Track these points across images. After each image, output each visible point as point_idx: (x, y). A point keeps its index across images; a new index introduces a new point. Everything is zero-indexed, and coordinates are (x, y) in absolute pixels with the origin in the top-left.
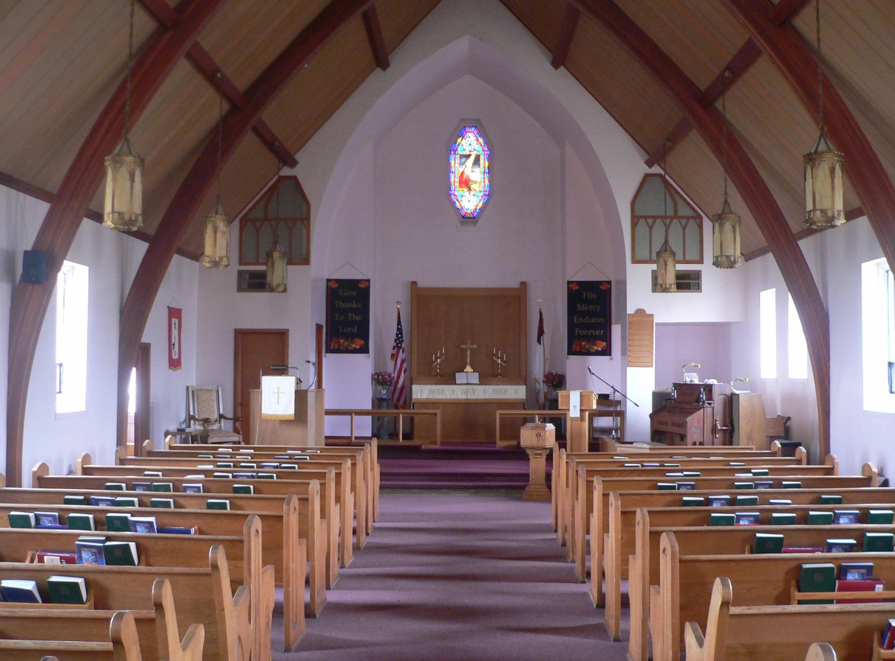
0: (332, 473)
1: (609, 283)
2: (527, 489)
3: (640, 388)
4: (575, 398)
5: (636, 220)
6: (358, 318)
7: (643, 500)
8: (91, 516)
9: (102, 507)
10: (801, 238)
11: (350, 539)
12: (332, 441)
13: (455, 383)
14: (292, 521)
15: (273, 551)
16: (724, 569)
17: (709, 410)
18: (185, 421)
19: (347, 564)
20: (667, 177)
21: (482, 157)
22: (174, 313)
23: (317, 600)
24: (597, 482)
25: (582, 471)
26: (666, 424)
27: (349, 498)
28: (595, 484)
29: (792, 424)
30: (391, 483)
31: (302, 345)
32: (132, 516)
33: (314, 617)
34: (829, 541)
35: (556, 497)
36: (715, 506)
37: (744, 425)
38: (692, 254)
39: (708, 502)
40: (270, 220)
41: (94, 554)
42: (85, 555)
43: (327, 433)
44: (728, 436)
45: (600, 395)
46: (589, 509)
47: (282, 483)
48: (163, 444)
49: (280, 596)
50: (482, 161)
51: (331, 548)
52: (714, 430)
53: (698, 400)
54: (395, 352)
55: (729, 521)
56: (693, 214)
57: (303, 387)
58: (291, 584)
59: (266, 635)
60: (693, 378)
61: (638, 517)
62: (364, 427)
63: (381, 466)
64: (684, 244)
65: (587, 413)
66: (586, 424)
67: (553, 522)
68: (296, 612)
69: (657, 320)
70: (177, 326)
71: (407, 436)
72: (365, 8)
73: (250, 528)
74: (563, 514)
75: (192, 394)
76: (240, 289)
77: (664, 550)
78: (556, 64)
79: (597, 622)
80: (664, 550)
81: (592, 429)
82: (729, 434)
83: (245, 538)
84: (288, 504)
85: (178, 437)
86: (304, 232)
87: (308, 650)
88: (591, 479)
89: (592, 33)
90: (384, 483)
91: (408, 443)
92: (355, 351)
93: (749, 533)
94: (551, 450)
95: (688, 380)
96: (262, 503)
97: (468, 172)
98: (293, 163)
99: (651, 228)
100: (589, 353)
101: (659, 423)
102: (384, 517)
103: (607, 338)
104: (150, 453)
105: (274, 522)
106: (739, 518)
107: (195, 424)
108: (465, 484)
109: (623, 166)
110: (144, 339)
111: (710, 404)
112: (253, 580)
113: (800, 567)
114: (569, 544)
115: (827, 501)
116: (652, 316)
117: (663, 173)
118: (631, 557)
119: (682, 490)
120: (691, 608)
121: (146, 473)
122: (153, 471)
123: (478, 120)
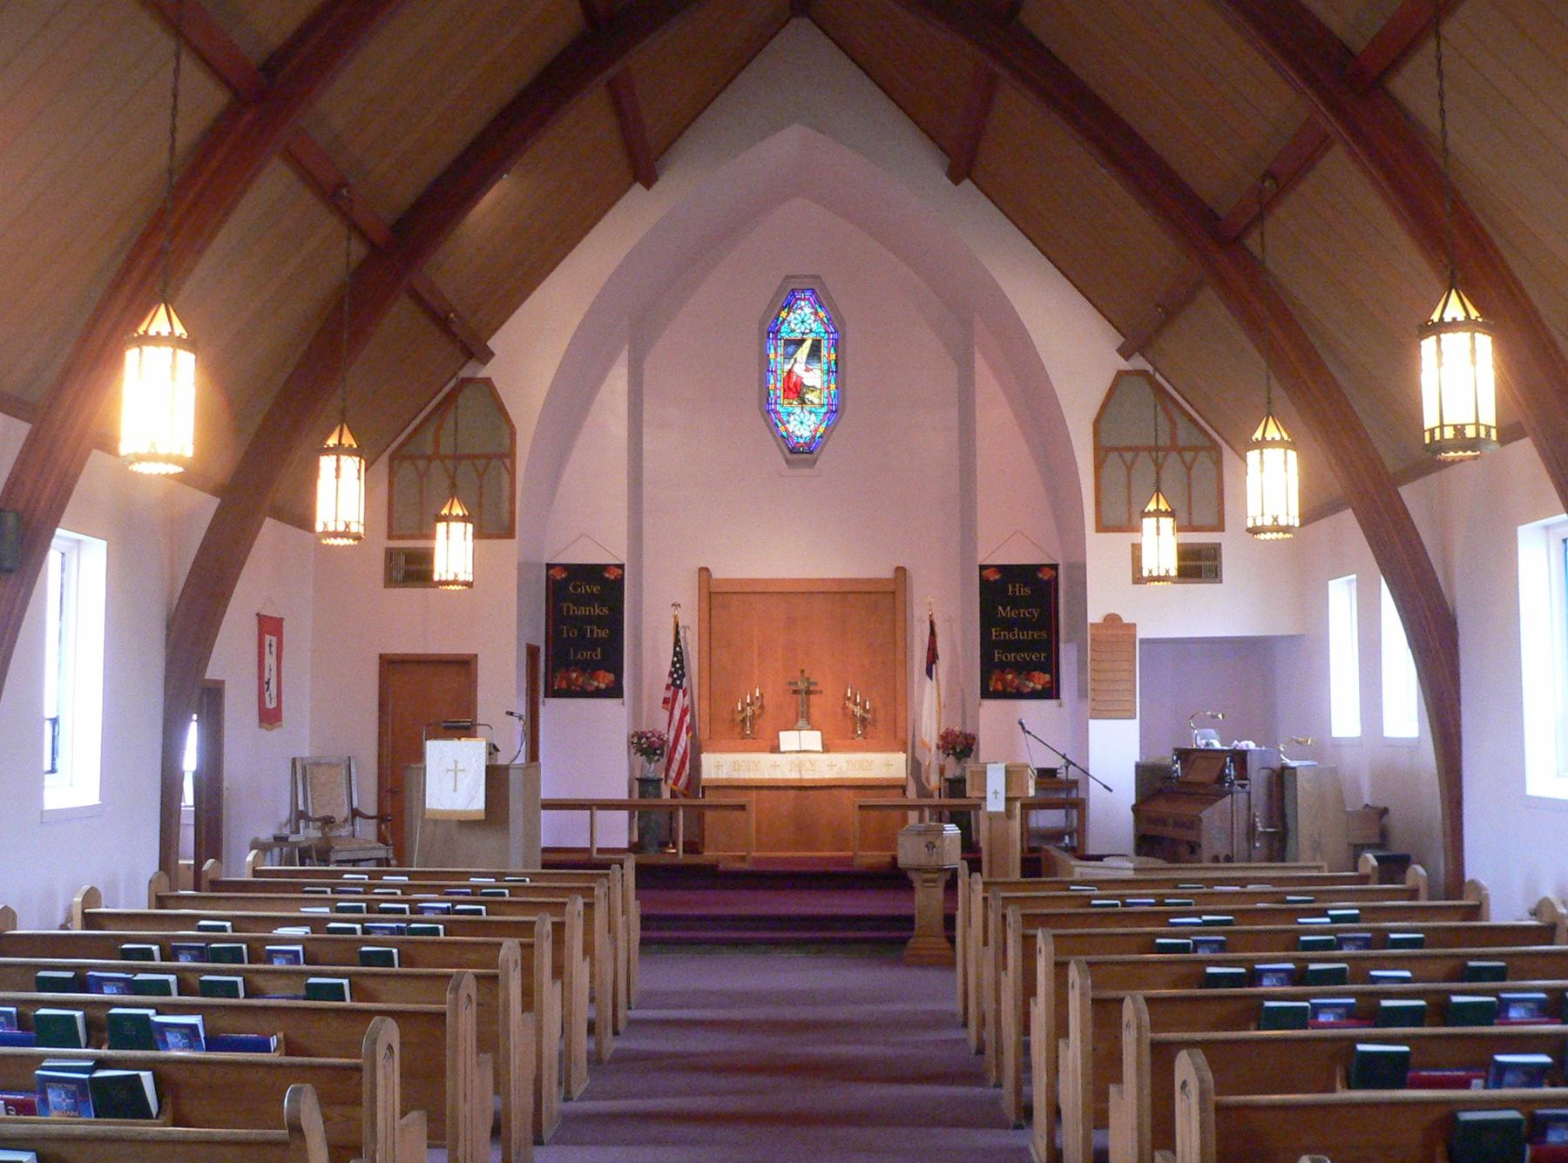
0: (544, 924)
1: (1055, 567)
2: (911, 943)
3: (1114, 754)
4: (996, 781)
6: (603, 634)
7: (1135, 975)
8: (78, 1014)
9: (108, 995)
10: (1401, 483)
11: (582, 1044)
12: (559, 861)
13: (775, 749)
14: (464, 1023)
17: (1241, 797)
18: (290, 820)
19: (577, 1091)
20: (1158, 377)
21: (824, 343)
22: (269, 626)
27: (580, 970)
28: (1041, 943)
29: (1395, 821)
30: (659, 934)
31: (500, 684)
32: (158, 1013)
34: (1500, 1058)
35: (965, 948)
36: (1268, 985)
37: (1306, 824)
38: (1203, 515)
39: (1254, 977)
41: (72, 1095)
42: (53, 1097)
44: (1276, 845)
47: (455, 943)
48: (244, 863)
50: (824, 352)
53: (1221, 778)
54: (669, 694)
57: (502, 759)
62: (616, 831)
63: (643, 905)
65: (1018, 805)
66: (1016, 824)
67: (959, 1007)
69: (1142, 633)
70: (274, 649)
71: (692, 847)
72: (611, 72)
73: (374, 1042)
74: (979, 986)
75: (301, 771)
76: (390, 581)
77: (1184, 1084)
78: (956, 176)
80: (1184, 1084)
81: (1026, 831)
82: (1279, 843)
83: (367, 1068)
84: (456, 989)
85: (276, 851)
86: (506, 477)
88: (1032, 932)
89: (1019, 114)
94: (954, 873)
95: (1201, 743)
97: (799, 369)
99: (1129, 468)
100: (1019, 695)
101: (1151, 821)
102: (648, 999)
104: (216, 885)
105: (425, 1029)
106: (1317, 1009)
107: (307, 827)
108: (796, 935)
109: (1076, 352)
110: (210, 674)
111: (1243, 786)
113: (1451, 1119)
114: (990, 1051)
115: (1478, 974)
117: (1150, 368)
118: (1113, 1089)
119: (1203, 954)
121: (202, 923)
122: (216, 918)
123: (817, 277)
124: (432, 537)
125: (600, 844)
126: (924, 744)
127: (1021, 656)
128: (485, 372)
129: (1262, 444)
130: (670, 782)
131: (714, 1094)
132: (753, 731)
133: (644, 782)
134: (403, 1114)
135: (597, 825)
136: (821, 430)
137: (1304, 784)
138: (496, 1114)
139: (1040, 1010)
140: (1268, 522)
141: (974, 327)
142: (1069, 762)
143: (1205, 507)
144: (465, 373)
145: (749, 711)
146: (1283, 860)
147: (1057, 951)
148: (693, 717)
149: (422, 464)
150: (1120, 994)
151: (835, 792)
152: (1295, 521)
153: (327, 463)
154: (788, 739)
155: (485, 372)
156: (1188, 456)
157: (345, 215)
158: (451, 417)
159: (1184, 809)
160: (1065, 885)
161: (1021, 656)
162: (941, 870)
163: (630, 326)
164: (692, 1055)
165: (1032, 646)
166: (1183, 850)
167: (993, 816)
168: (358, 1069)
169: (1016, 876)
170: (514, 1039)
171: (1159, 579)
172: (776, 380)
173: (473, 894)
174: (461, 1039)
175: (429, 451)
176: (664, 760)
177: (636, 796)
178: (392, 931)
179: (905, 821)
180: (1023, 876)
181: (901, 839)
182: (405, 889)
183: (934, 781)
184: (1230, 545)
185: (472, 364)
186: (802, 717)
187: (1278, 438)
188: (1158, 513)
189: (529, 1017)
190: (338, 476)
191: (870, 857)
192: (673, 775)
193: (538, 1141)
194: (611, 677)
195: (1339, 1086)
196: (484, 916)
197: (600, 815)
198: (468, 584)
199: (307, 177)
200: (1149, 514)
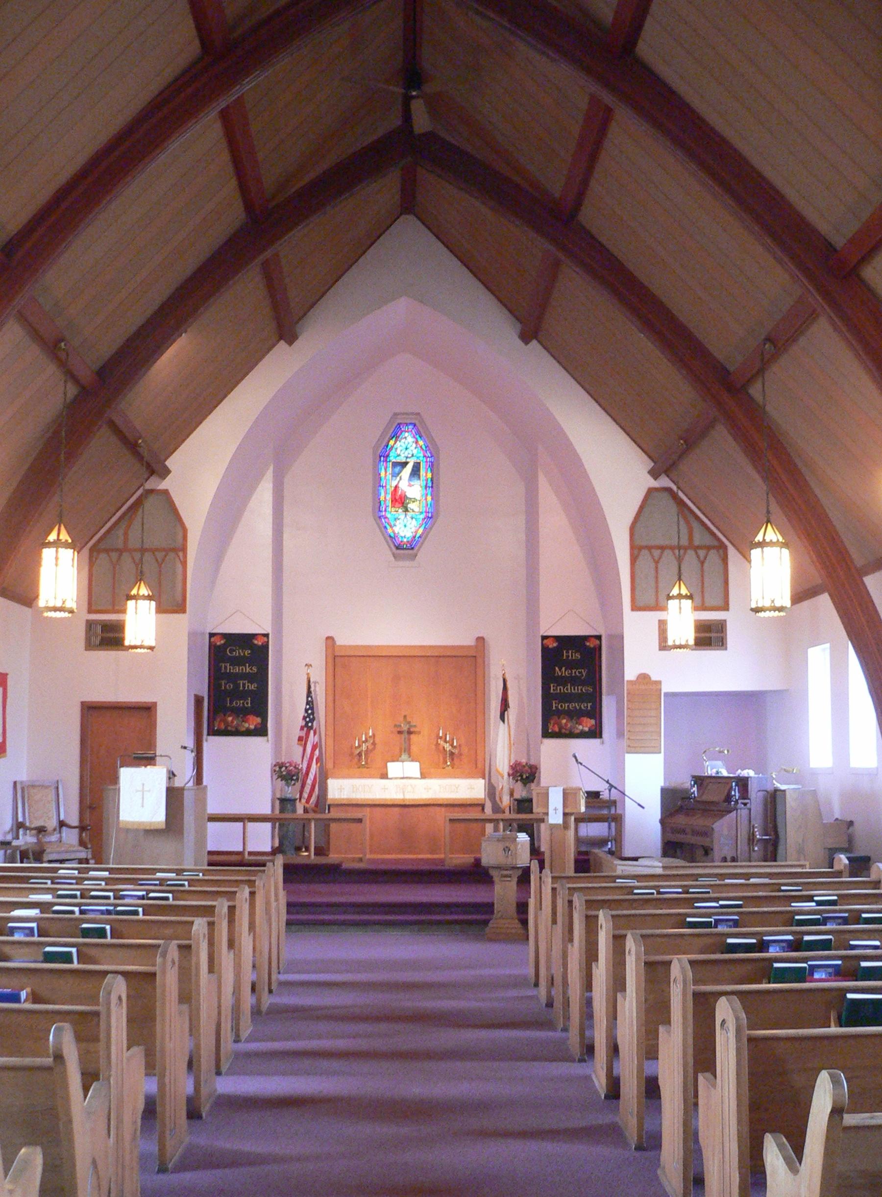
0: (222, 906)
2: (490, 925)
3: (644, 781)
5: (636, 552)
6: (253, 687)
7: (676, 945)
10: (867, 574)
11: (248, 1000)
12: (219, 860)
13: (384, 776)
14: (169, 981)
15: (143, 1025)
16: (825, 1054)
17: (744, 812)
18: (12, 829)
19: (244, 1034)
20: (681, 494)
21: (423, 466)
23: (204, 1091)
24: (603, 918)
25: (578, 901)
26: (683, 831)
27: (246, 942)
29: (859, 829)
30: (302, 917)
31: (174, 725)
33: (200, 1117)
36: (773, 952)
37: (793, 834)
39: (762, 946)
40: (130, 551)
43: (210, 848)
44: (770, 848)
45: (587, 792)
46: (591, 955)
47: (152, 922)
49: (151, 1086)
50: (422, 472)
51: (223, 1012)
52: (751, 839)
53: (728, 798)
55: (800, 975)
56: (716, 543)
57: (178, 783)
58: (167, 1074)
59: (131, 1152)
60: (716, 768)
61: (675, 971)
62: (262, 838)
63: (289, 893)
64: (703, 587)
65: (573, 818)
66: (571, 833)
67: (531, 971)
68: (175, 1112)
69: (665, 689)
71: (320, 851)
72: (268, 254)
73: (109, 993)
75: (21, 791)
78: (530, 333)
79: (617, 1128)
81: (578, 840)
82: (772, 849)
84: (164, 955)
86: (179, 567)
87: (193, 1169)
90: (293, 917)
91: (322, 860)
92: (248, 733)
93: (834, 994)
95: (711, 772)
96: (122, 953)
98: (165, 472)
100: (571, 735)
101: (675, 831)
102: (293, 966)
103: (596, 713)
105: (142, 983)
106: (813, 968)
107: (25, 834)
109: (617, 473)
111: (745, 804)
112: (113, 1073)
116: (660, 682)
117: (675, 488)
118: (662, 1029)
119: (721, 929)
120: (772, 1109)
123: (418, 414)
124: (124, 611)
125: (250, 848)
126: (497, 770)
127: (572, 706)
128: (163, 485)
129: (762, 544)
130: (303, 801)
131: (349, 1037)
132: (365, 762)
133: (284, 801)
134: (128, 1049)
135: (248, 834)
136: (421, 531)
137: (791, 802)
138: (191, 1052)
139: (601, 971)
140: (767, 604)
141: (536, 452)
142: (611, 786)
143: (714, 592)
144: (149, 485)
145: (364, 747)
146: (775, 861)
147: (615, 927)
148: (320, 752)
149: (114, 555)
150: (667, 958)
151: (431, 809)
152: (787, 603)
153: (48, 554)
154: (393, 768)
155: (163, 485)
156: (702, 553)
157: (62, 363)
158: (138, 519)
159: (698, 821)
160: (614, 878)
161: (572, 706)
162: (514, 868)
163: (276, 449)
164: (325, 1008)
165: (580, 698)
166: (700, 852)
167: (553, 827)
168: (97, 1014)
169: (571, 872)
170: (203, 991)
171: (680, 647)
172: (386, 493)
173: (160, 885)
174: (167, 994)
175: (120, 544)
176: (299, 785)
177: (277, 811)
178: (102, 912)
179: (483, 833)
180: (576, 872)
181: (484, 845)
182: (107, 880)
183: (506, 801)
184: (734, 621)
185: (153, 479)
186: (406, 751)
187: (775, 540)
188: (680, 596)
189: (214, 977)
190: (56, 565)
191: (459, 859)
192: (305, 795)
193: (218, 1073)
194: (259, 720)
195: (832, 1024)
196: (171, 902)
197: (250, 825)
198: (151, 648)
199: (36, 335)
200: (673, 598)
